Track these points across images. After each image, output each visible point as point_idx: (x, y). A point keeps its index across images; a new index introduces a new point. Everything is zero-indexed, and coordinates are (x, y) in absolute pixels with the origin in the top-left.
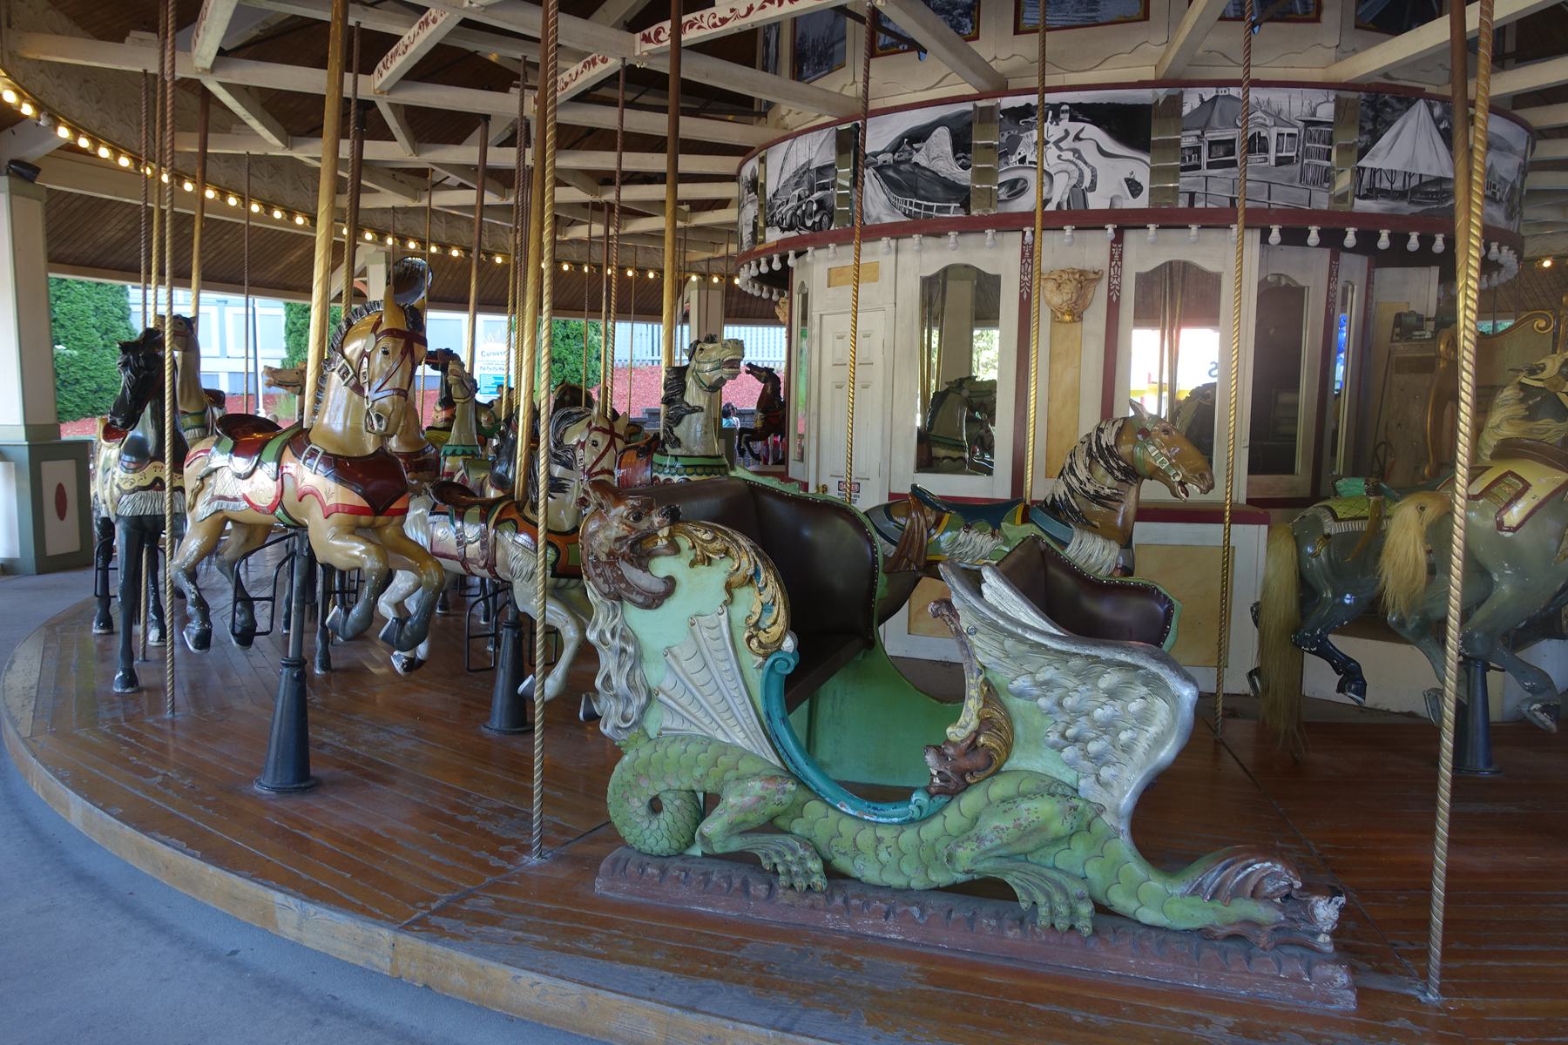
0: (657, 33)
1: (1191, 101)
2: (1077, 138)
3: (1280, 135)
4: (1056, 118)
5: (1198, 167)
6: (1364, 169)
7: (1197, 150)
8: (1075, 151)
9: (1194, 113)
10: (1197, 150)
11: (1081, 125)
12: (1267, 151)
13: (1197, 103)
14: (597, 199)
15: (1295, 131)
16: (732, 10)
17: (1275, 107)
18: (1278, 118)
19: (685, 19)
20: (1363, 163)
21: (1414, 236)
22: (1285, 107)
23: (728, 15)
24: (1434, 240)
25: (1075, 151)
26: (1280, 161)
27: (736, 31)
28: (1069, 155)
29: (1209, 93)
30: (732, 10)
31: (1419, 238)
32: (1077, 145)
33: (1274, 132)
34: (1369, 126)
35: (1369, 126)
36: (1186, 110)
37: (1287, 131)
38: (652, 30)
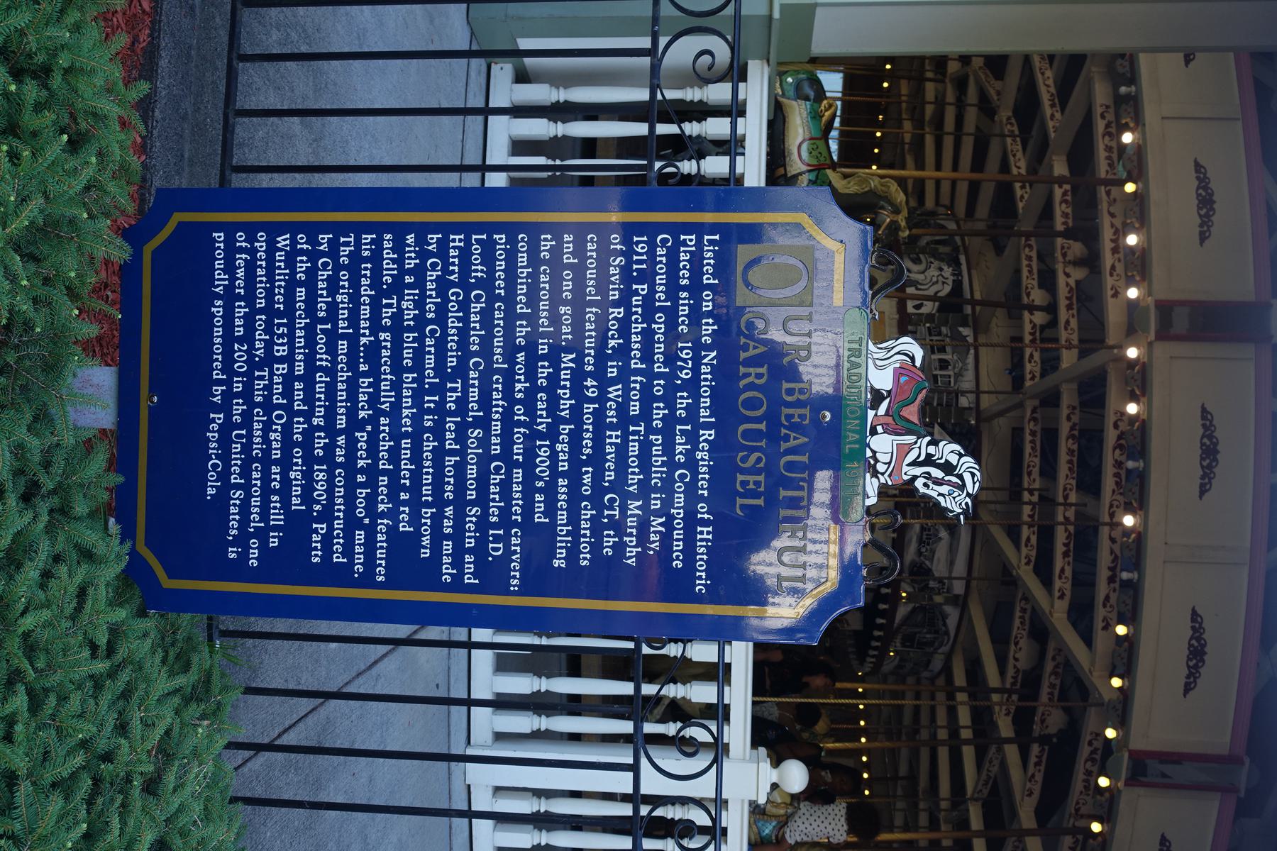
0: (1011, 124)
1: (965, 331)
2: (944, 283)
3: (950, 376)
4: (953, 275)
5: (930, 334)
6: (933, 427)
7: (940, 334)
8: (937, 282)
9: (960, 333)
10: (940, 334)
11: (951, 284)
12: (941, 369)
13: (965, 334)
14: (903, 112)
15: (952, 384)
16: (1115, 200)
17: (965, 373)
18: (958, 375)
19: (1018, 139)
20: (936, 426)
21: (881, 633)
22: (965, 379)
23: (1112, 197)
24: (883, 618)
25: (937, 282)
26: (935, 377)
27: (1099, 196)
28: (934, 279)
29: (970, 339)
30: (1115, 200)
31: (885, 609)
32: (940, 283)
33: (951, 373)
34: (957, 430)
35: (957, 430)
36: (961, 329)
37: (952, 380)
38: (1013, 121)
